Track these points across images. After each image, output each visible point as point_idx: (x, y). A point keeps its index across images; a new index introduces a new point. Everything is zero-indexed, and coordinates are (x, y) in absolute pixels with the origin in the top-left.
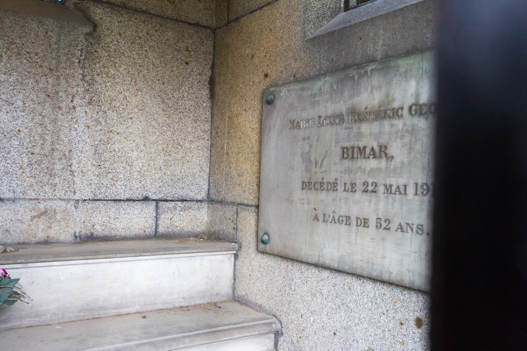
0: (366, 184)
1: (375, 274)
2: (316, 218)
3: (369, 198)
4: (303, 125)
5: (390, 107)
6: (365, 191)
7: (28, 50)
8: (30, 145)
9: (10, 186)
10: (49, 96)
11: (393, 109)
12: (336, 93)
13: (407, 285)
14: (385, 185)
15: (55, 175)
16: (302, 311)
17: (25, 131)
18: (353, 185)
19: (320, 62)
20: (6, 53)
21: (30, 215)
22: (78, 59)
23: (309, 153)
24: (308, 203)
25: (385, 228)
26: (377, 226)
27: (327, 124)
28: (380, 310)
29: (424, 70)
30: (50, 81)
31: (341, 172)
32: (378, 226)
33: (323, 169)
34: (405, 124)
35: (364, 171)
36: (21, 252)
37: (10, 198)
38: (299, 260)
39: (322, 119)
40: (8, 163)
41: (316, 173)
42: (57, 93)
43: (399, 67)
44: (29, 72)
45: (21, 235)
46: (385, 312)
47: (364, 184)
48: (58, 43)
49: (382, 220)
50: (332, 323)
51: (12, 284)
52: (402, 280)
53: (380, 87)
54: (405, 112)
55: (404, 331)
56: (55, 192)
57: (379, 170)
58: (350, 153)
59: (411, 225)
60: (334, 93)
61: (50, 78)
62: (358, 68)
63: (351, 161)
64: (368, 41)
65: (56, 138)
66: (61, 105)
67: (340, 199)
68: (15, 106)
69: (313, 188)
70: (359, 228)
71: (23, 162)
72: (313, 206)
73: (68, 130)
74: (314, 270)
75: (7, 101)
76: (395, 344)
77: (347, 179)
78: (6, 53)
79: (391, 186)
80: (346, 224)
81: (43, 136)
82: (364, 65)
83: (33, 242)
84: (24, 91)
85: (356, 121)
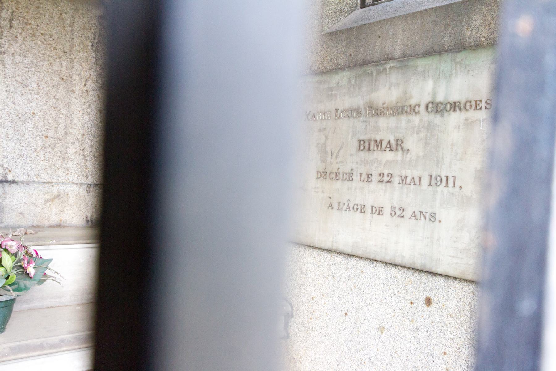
0: (381, 174)
1: (387, 259)
2: (331, 206)
3: (384, 188)
4: (319, 117)
5: (407, 104)
6: (381, 182)
7: (43, 32)
8: (44, 129)
9: (24, 169)
10: (63, 79)
11: (410, 106)
12: (354, 88)
13: (419, 268)
14: (401, 177)
15: (68, 159)
16: (313, 294)
17: (39, 114)
18: (369, 175)
19: (337, 57)
20: (21, 34)
21: (43, 199)
22: (91, 42)
23: (325, 144)
24: (323, 192)
25: (399, 216)
26: (391, 214)
27: (344, 117)
28: (392, 291)
29: (441, 71)
30: (64, 63)
31: (357, 163)
32: (393, 214)
33: (339, 160)
34: (421, 120)
35: (380, 163)
36: (40, 234)
37: (24, 181)
38: (312, 245)
39: (339, 112)
40: (22, 146)
41: (331, 163)
42: (71, 76)
43: (417, 67)
44: (44, 54)
45: (35, 218)
46: (396, 293)
47: (380, 175)
48: (72, 25)
49: (397, 208)
50: (343, 304)
51: (46, 264)
52: (414, 263)
53: (398, 84)
54: (422, 109)
55: (413, 310)
56: (67, 176)
57: (395, 162)
58: (367, 145)
59: (425, 214)
60: (352, 87)
61: (64, 61)
62: (377, 65)
63: (367, 153)
64: (386, 40)
65: (69, 121)
66: (74, 89)
67: (355, 189)
68: (29, 88)
69: (328, 177)
70: (374, 215)
71: (37, 144)
72: (328, 195)
73: (81, 114)
74: (326, 255)
75: (21, 83)
76: (405, 321)
77: (363, 170)
78: (21, 34)
79: (406, 177)
80: (361, 212)
81: (57, 119)
82: (382, 62)
83: (46, 225)
84: (38, 74)
85: (373, 115)
